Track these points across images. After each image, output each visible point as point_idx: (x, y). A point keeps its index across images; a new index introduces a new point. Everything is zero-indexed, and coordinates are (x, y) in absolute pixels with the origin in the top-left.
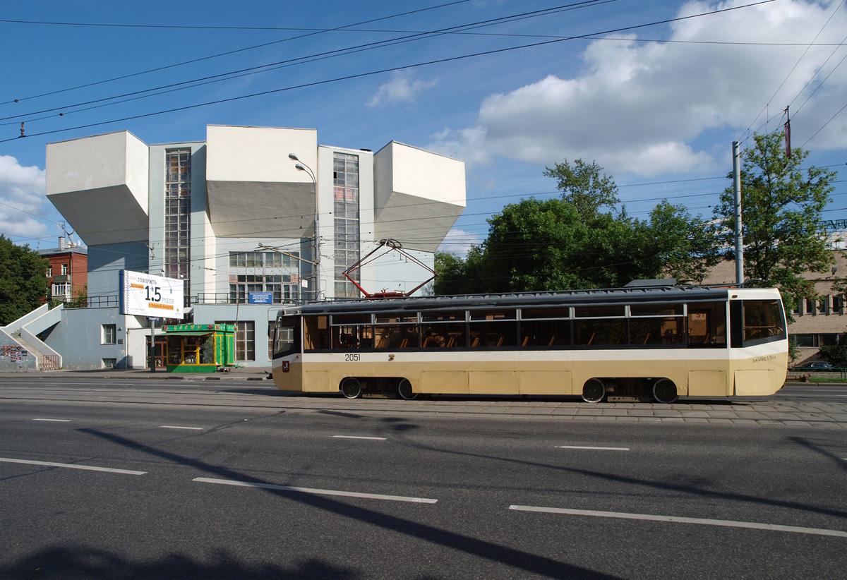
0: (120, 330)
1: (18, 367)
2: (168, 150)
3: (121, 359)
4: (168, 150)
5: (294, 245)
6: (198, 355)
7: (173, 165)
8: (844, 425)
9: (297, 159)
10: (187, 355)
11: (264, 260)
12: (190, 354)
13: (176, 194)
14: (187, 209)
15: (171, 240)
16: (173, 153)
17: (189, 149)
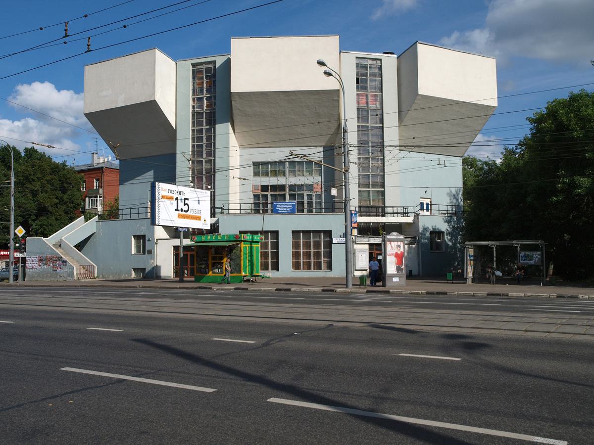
3: (150, 269)
4: (194, 65)
10: (214, 265)
13: (202, 107)
14: (212, 122)
16: (199, 67)
17: (214, 62)
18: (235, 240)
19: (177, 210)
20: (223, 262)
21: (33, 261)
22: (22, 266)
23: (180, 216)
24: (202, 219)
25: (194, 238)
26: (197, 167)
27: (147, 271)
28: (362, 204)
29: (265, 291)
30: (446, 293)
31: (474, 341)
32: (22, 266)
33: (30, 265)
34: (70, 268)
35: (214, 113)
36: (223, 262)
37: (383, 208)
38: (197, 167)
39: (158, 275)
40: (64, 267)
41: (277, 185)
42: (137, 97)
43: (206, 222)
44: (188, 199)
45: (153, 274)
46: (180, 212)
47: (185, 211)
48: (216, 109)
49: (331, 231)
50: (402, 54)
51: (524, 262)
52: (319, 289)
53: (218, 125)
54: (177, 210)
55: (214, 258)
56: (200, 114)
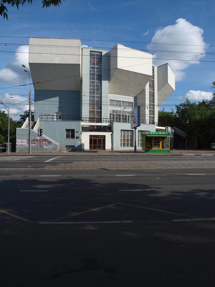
0: (77, 132)
1: (45, 150)
2: (91, 51)
3: (77, 146)
4: (91, 51)
5: (131, 99)
6: (161, 145)
7: (93, 58)
8: (214, 174)
9: (25, 67)
10: (155, 145)
11: (121, 104)
12: (157, 145)
13: (94, 71)
14: (100, 79)
15: (92, 92)
16: (93, 53)
17: (101, 53)
18: (168, 134)
20: (160, 144)
21: (22, 141)
22: (10, 144)
26: (92, 99)
27: (75, 147)
28: (91, 117)
29: (209, 156)
31: (72, 178)
32: (10, 144)
33: (20, 144)
34: (55, 145)
35: (101, 75)
36: (160, 144)
37: (101, 119)
38: (92, 99)
39: (82, 148)
40: (49, 145)
42: (79, 63)
45: (80, 148)
49: (74, 130)
55: (155, 142)
56: (94, 75)
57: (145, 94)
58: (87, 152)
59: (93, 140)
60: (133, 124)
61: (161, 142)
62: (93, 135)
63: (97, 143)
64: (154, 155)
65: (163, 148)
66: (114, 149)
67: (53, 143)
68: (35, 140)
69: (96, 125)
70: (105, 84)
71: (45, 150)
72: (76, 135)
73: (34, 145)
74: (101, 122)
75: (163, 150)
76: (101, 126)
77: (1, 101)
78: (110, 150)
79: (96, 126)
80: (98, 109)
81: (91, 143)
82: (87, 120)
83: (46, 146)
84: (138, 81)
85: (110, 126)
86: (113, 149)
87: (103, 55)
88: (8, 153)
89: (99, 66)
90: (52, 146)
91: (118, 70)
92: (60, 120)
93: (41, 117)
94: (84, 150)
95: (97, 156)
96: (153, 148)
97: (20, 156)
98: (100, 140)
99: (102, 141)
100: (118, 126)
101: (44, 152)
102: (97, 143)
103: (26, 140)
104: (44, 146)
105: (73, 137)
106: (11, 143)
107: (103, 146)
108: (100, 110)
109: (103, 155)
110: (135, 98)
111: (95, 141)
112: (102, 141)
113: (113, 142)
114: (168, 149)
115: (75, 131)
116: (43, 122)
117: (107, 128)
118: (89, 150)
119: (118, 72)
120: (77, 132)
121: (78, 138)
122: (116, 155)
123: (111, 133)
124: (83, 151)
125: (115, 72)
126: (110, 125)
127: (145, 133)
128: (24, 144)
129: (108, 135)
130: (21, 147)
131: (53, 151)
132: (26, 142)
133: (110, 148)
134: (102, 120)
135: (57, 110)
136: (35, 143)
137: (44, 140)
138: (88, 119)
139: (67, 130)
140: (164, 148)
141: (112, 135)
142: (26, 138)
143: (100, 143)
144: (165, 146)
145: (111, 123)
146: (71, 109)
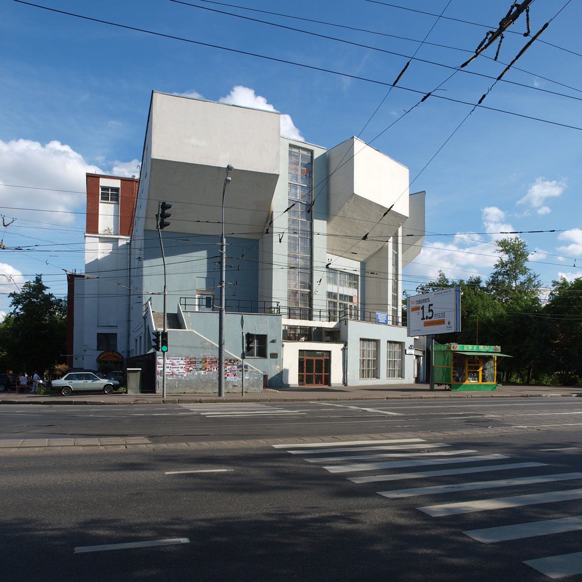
0: (273, 341)
1: (230, 386)
5: (353, 266)
17: (312, 152)
19: (423, 319)
20: (479, 372)
21: (172, 364)
23: (426, 324)
24: (446, 322)
25: (456, 347)
30: (542, 396)
36: (479, 372)
37: (311, 311)
41: (288, 243)
43: (451, 324)
44: (432, 305)
45: (277, 382)
46: (426, 320)
47: (430, 318)
48: (261, 361)
50: (146, 135)
51: (452, 377)
52: (459, 236)
53: (326, 239)
54: (423, 319)
55: (470, 367)
57: (272, 253)
58: (294, 390)
59: (305, 363)
60: (424, 326)
61: (481, 369)
62: (306, 350)
63: (315, 368)
64: (492, 397)
65: (484, 380)
66: (349, 384)
67: (251, 368)
68: (206, 362)
69: (300, 326)
70: (320, 226)
71: (230, 386)
72: (270, 349)
73: (203, 374)
74: (310, 319)
75: (484, 385)
76: (311, 328)
77: (330, 260)
78: (340, 386)
79: (300, 329)
80: (304, 287)
81: (301, 369)
82: (324, 317)
83: (235, 376)
84: (380, 228)
85: (339, 328)
86: (347, 383)
87: (316, 156)
88: (163, 396)
89: (306, 184)
90: (248, 378)
91: (353, 199)
92: (209, 310)
93: (183, 301)
94: (288, 386)
95: (384, 398)
96: (467, 382)
97: (207, 402)
98: (319, 362)
99: (324, 363)
100: (356, 330)
101: (228, 392)
102: (315, 368)
103: (182, 362)
104: (228, 376)
105: (262, 353)
106: (140, 369)
107: (322, 373)
108: (309, 291)
109: (396, 398)
110: (363, 264)
111: (309, 362)
112: (324, 363)
113: (344, 367)
114: (492, 383)
115: (269, 340)
116: (189, 315)
117: (324, 334)
118: (298, 386)
119: (351, 202)
120: (273, 341)
121: (274, 356)
122: (421, 398)
123: (342, 346)
124: (285, 387)
125: (347, 201)
126: (336, 329)
127: (453, 347)
128: (177, 372)
129: (335, 349)
130: (170, 379)
131: (251, 388)
132: (182, 366)
133: (341, 382)
134: (315, 313)
135: (202, 284)
136: (206, 369)
137: (230, 361)
138: (325, 314)
139: (250, 337)
140: (486, 382)
141: (344, 350)
142: (182, 356)
143: (319, 370)
144: (487, 377)
145: (344, 322)
146: (240, 282)
